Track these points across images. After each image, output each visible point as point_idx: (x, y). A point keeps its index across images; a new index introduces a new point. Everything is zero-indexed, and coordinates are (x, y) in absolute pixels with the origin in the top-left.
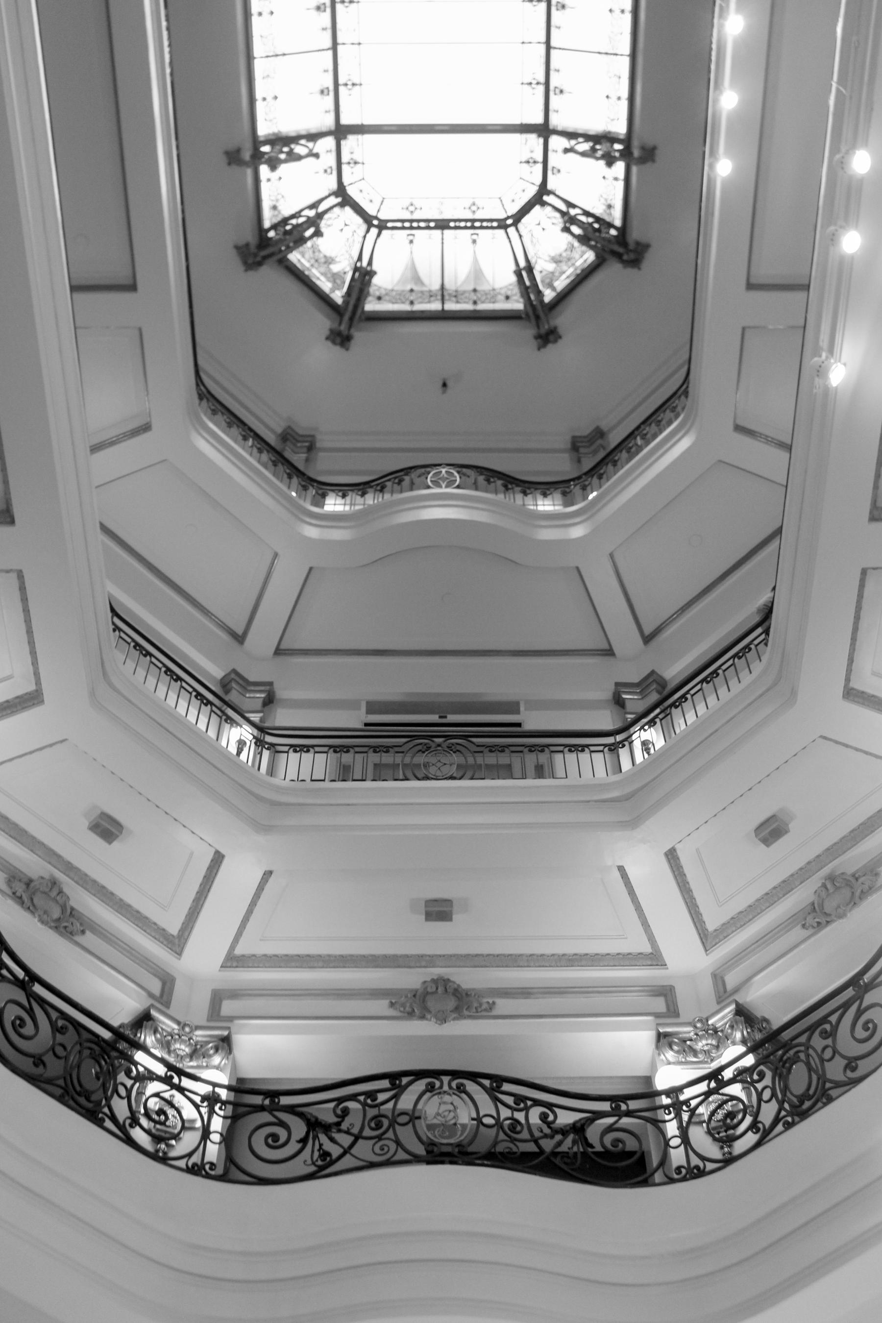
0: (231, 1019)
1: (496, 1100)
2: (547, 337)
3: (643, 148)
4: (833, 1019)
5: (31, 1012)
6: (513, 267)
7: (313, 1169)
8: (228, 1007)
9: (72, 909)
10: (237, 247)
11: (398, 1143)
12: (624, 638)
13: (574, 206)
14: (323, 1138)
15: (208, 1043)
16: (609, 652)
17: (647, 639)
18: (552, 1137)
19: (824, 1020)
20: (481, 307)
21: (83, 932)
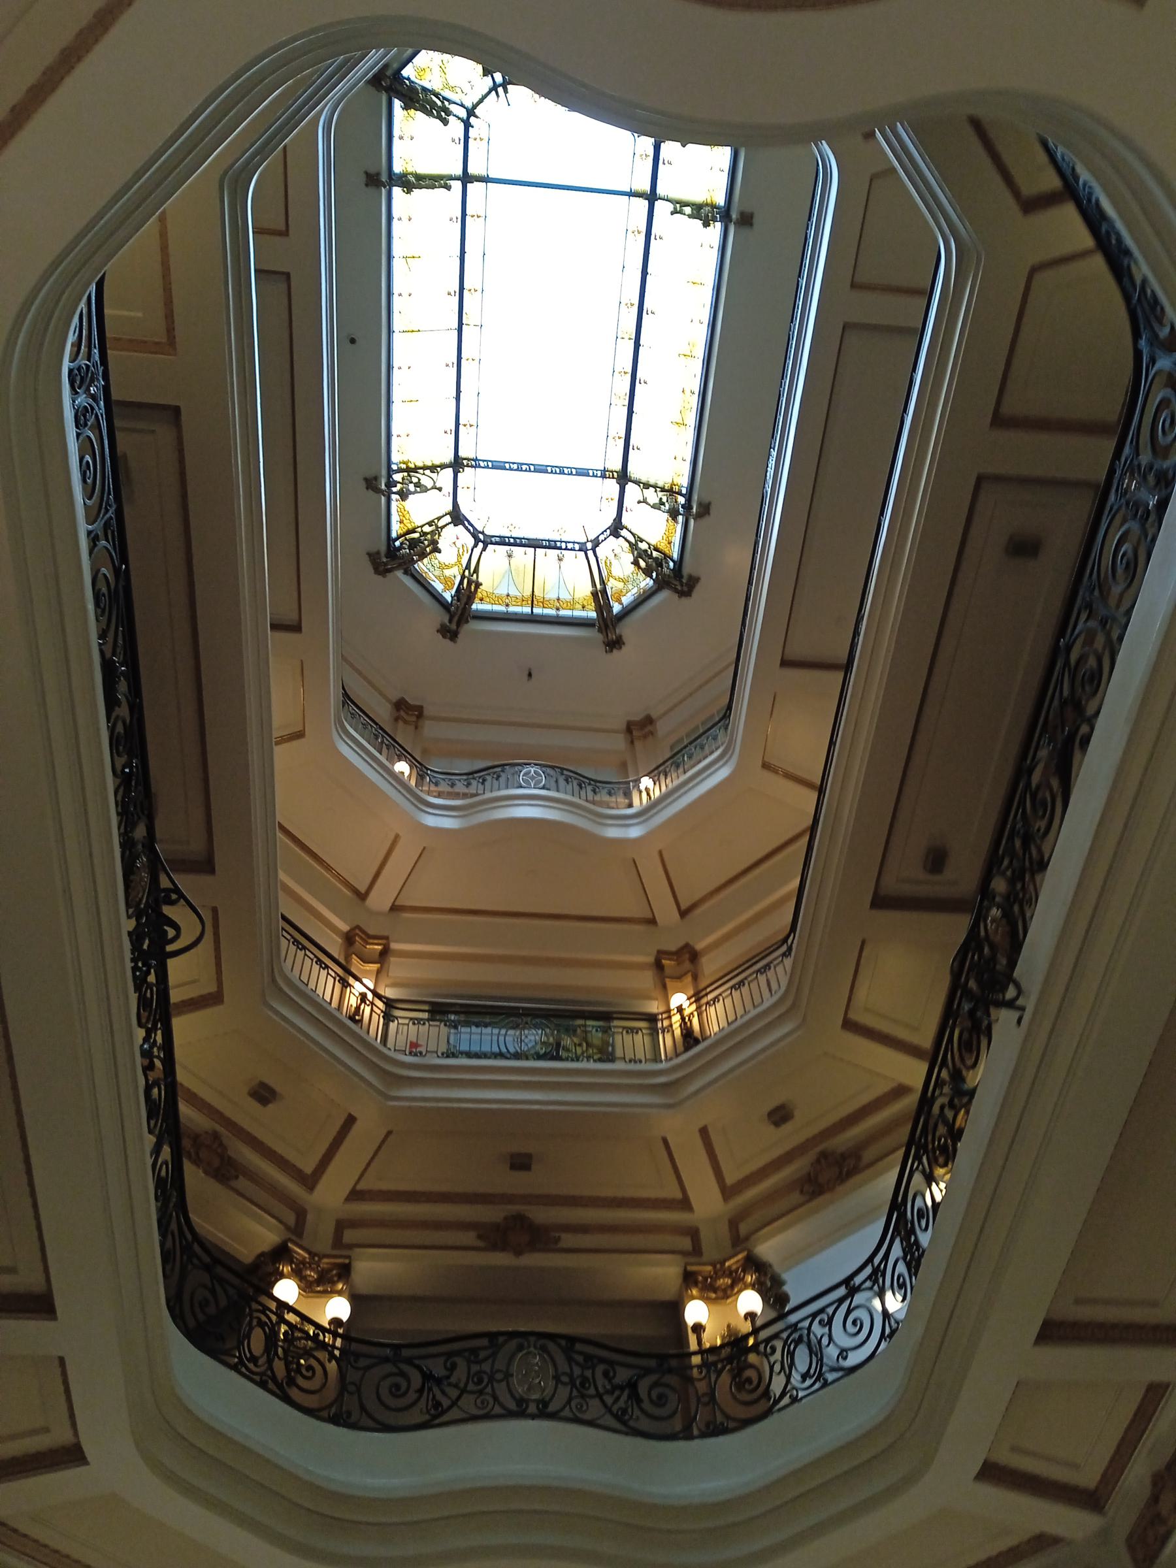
0: (351, 1247)
1: (570, 1360)
2: (614, 644)
3: (700, 504)
4: (830, 1310)
5: (213, 1292)
6: (590, 588)
7: (427, 1417)
8: (349, 1236)
9: (230, 1158)
10: (369, 554)
11: (496, 1399)
12: (666, 913)
13: (642, 541)
14: (436, 1390)
15: (331, 1270)
16: (652, 921)
17: (683, 914)
18: (612, 1393)
19: (822, 1310)
20: (562, 613)
21: (237, 1177)
